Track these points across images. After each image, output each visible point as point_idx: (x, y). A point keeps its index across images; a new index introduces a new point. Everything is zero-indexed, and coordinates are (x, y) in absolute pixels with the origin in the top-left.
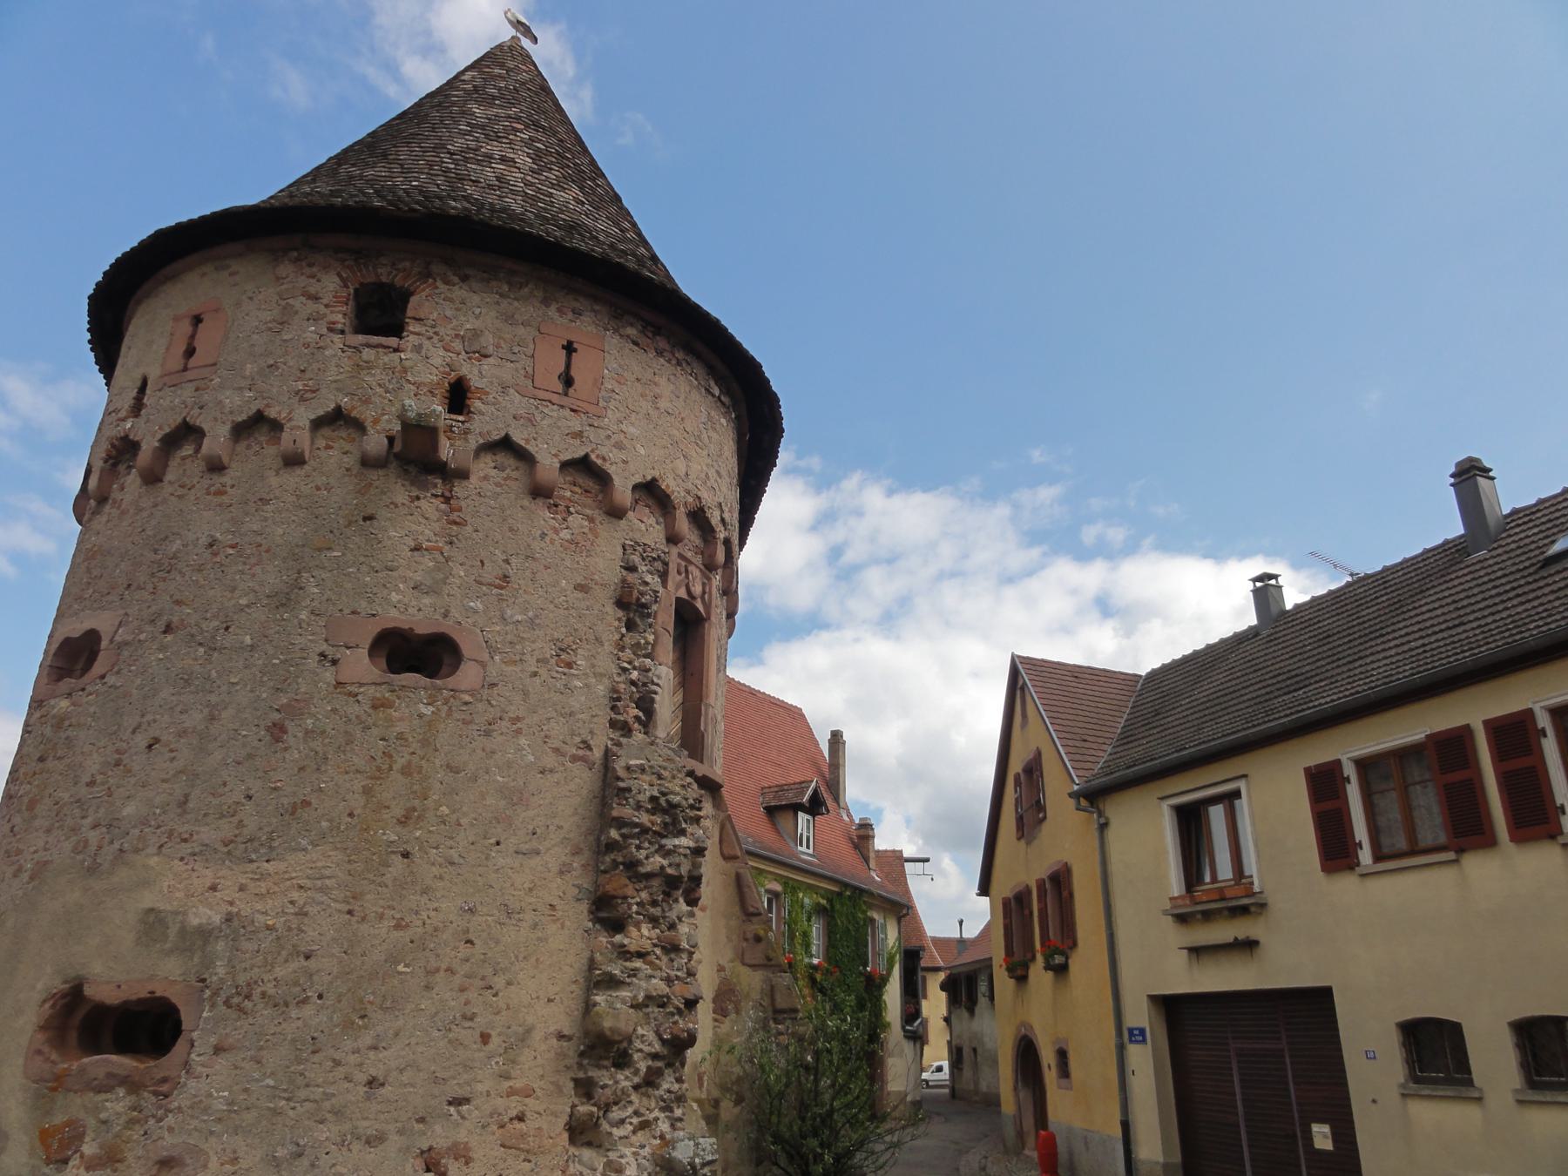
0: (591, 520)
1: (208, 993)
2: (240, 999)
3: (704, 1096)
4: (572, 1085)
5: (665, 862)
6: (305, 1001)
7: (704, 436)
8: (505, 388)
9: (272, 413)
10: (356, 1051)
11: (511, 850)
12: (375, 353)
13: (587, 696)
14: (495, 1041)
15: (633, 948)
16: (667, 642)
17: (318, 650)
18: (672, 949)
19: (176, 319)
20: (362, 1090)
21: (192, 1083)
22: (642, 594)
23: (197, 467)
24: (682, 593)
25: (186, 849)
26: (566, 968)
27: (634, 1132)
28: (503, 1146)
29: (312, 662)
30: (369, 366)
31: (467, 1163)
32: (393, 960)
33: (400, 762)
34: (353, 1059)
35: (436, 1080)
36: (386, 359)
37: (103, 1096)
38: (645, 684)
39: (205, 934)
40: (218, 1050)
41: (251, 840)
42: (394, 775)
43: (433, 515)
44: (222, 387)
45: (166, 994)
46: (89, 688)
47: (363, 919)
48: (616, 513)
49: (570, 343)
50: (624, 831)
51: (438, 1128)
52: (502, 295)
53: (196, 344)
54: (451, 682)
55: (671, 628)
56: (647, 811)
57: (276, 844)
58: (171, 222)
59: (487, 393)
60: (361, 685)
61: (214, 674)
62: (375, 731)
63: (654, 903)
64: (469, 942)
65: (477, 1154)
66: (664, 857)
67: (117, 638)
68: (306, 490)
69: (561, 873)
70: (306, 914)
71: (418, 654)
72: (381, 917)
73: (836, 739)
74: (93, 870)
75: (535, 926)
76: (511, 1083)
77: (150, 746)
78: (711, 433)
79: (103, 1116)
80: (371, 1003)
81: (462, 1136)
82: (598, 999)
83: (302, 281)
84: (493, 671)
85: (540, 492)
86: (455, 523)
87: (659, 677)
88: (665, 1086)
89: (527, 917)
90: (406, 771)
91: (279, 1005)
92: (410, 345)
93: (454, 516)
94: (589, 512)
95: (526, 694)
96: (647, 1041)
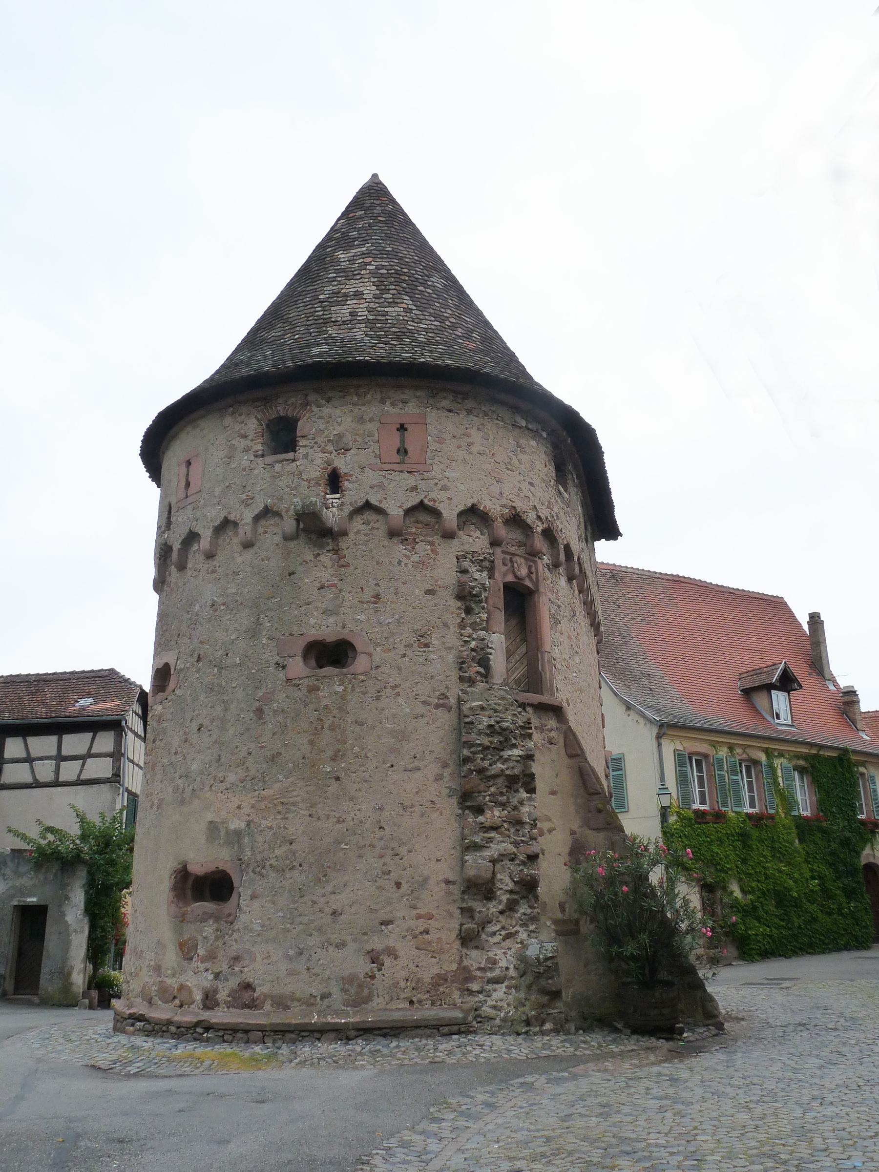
0: (432, 544)
2: (261, 868)
4: (459, 911)
5: (503, 767)
6: (293, 868)
7: (515, 461)
8: (363, 468)
9: (232, 517)
10: (324, 895)
12: (282, 466)
13: (441, 664)
14: (405, 887)
15: (487, 824)
17: (275, 661)
18: (518, 823)
19: (179, 465)
20: (328, 919)
23: (200, 558)
24: (510, 578)
25: (222, 787)
27: (504, 940)
31: (395, 959)
32: (338, 842)
34: (322, 900)
35: (371, 910)
36: (289, 468)
37: (203, 924)
38: (482, 649)
39: (238, 833)
40: (253, 897)
43: (329, 563)
44: (205, 505)
46: (169, 698)
47: (319, 819)
48: (449, 535)
50: (473, 749)
51: (376, 939)
52: (354, 405)
53: (190, 480)
55: (501, 605)
56: (487, 735)
58: (149, 422)
59: (351, 476)
60: (300, 679)
62: (311, 706)
63: (502, 794)
65: (401, 953)
67: (178, 667)
69: (436, 780)
70: (287, 818)
71: (332, 654)
72: (328, 817)
73: (815, 620)
74: (183, 802)
75: (422, 815)
80: (329, 867)
81: (391, 943)
82: (467, 858)
83: (237, 427)
84: (376, 658)
85: (393, 534)
86: (343, 566)
87: (492, 643)
88: (522, 911)
90: (332, 728)
92: (301, 455)
93: (342, 562)
94: (430, 539)
95: (399, 669)
96: (505, 882)
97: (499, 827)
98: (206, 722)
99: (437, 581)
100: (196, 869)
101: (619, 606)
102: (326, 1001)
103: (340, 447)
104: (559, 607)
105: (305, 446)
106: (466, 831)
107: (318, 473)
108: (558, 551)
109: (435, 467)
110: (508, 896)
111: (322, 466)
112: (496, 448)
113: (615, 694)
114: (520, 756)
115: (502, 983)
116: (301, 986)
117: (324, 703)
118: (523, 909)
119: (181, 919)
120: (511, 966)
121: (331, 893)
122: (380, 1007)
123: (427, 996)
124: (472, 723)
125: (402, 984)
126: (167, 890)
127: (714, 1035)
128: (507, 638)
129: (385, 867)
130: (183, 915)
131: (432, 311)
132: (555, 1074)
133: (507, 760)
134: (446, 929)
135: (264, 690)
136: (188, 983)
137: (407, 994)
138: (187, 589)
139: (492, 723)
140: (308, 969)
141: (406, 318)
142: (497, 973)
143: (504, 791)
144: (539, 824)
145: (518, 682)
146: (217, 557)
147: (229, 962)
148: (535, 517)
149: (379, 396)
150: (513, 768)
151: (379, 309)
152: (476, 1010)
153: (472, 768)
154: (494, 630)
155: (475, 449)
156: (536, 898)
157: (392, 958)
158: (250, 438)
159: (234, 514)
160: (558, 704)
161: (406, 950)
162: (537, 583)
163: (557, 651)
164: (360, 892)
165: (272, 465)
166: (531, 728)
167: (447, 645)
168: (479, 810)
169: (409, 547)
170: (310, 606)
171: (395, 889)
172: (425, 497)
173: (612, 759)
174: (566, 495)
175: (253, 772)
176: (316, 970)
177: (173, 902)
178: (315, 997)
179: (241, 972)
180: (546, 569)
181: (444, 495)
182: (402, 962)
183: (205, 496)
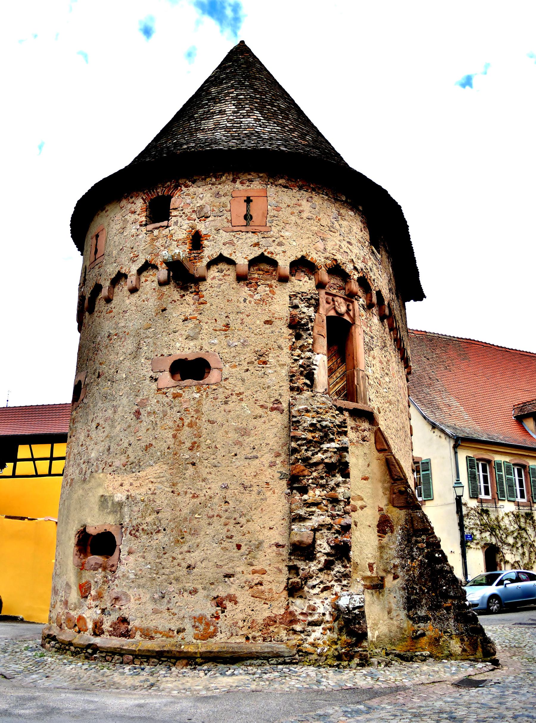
0: (270, 286)
1: (123, 529)
3: (374, 575)
4: (287, 568)
5: (323, 457)
6: (159, 531)
7: (336, 224)
9: (123, 271)
10: (181, 553)
11: (243, 457)
13: (277, 375)
14: (244, 549)
15: (310, 501)
16: (323, 343)
18: (334, 501)
20: (185, 571)
21: (122, 567)
22: (302, 319)
23: (103, 302)
24: (332, 313)
25: (110, 469)
26: (278, 513)
28: (253, 596)
29: (148, 381)
30: (157, 238)
31: (235, 604)
33: (187, 422)
34: (180, 557)
35: (218, 566)
36: (164, 232)
38: (308, 366)
39: (120, 505)
40: (130, 553)
41: (132, 463)
42: (186, 428)
43: (191, 302)
45: (110, 530)
47: (178, 494)
48: (283, 279)
49: (248, 198)
50: (299, 442)
52: (213, 184)
54: (206, 381)
57: (141, 464)
59: (210, 236)
60: (168, 388)
61: (114, 393)
62: (175, 409)
63: (322, 478)
64: (226, 502)
66: (323, 454)
68: (139, 303)
69: (270, 466)
70: (155, 494)
71: (192, 369)
72: (186, 493)
75: (259, 493)
76: (254, 568)
77: (97, 428)
78: (341, 222)
79: (95, 580)
80: (186, 532)
81: (232, 591)
82: (293, 527)
83: (129, 206)
85: (241, 278)
86: (202, 303)
87: (316, 361)
88: (336, 569)
89: (254, 489)
90: (190, 425)
91: (149, 534)
92: (173, 222)
93: (201, 300)
95: (243, 380)
96: (323, 546)
97: (320, 504)
98: (101, 422)
99: (274, 314)
100: (91, 531)
101: (428, 359)
102: (181, 635)
103: (201, 216)
104: (372, 338)
105: (175, 216)
106: (293, 506)
107: (185, 236)
108: (371, 294)
109: (273, 228)
110: (326, 558)
111: (188, 230)
112: (321, 215)
113: (425, 418)
114: (336, 448)
115: (320, 625)
116: (163, 622)
117: (185, 406)
118: (338, 568)
119: (82, 567)
120: (327, 613)
121: (186, 552)
122: (222, 641)
123: (260, 633)
124: (298, 422)
125: (241, 624)
126: (73, 545)
127: (491, 670)
128: (330, 359)
129: (229, 533)
130: (83, 564)
131: (275, 121)
132: (352, 706)
133: (326, 451)
134: (277, 581)
135: (141, 397)
136: (84, 615)
137: (245, 631)
138: (94, 326)
139: (315, 422)
140: (168, 609)
141: (255, 125)
142: (315, 617)
143: (324, 475)
144: (352, 502)
145: (338, 393)
146: (113, 301)
147: (112, 601)
148: (352, 267)
149: (231, 178)
150: (331, 457)
151: (236, 120)
152: (299, 646)
153: (299, 457)
154: (318, 351)
155: (305, 215)
156: (349, 560)
157: (232, 604)
158: (138, 213)
159: (125, 268)
160: (370, 410)
161: (244, 597)
162: (353, 319)
163: (370, 371)
164: (209, 552)
165: (152, 231)
166: (346, 427)
167: (281, 362)
168: (304, 490)
169: (252, 289)
170: (177, 334)
171: (236, 550)
172: (265, 251)
173: (422, 463)
174: (379, 256)
175: (132, 459)
176: (175, 611)
177: (76, 555)
178: (173, 631)
179: (120, 609)
180: (361, 309)
181: (280, 249)
182: (240, 606)
183: (106, 257)
